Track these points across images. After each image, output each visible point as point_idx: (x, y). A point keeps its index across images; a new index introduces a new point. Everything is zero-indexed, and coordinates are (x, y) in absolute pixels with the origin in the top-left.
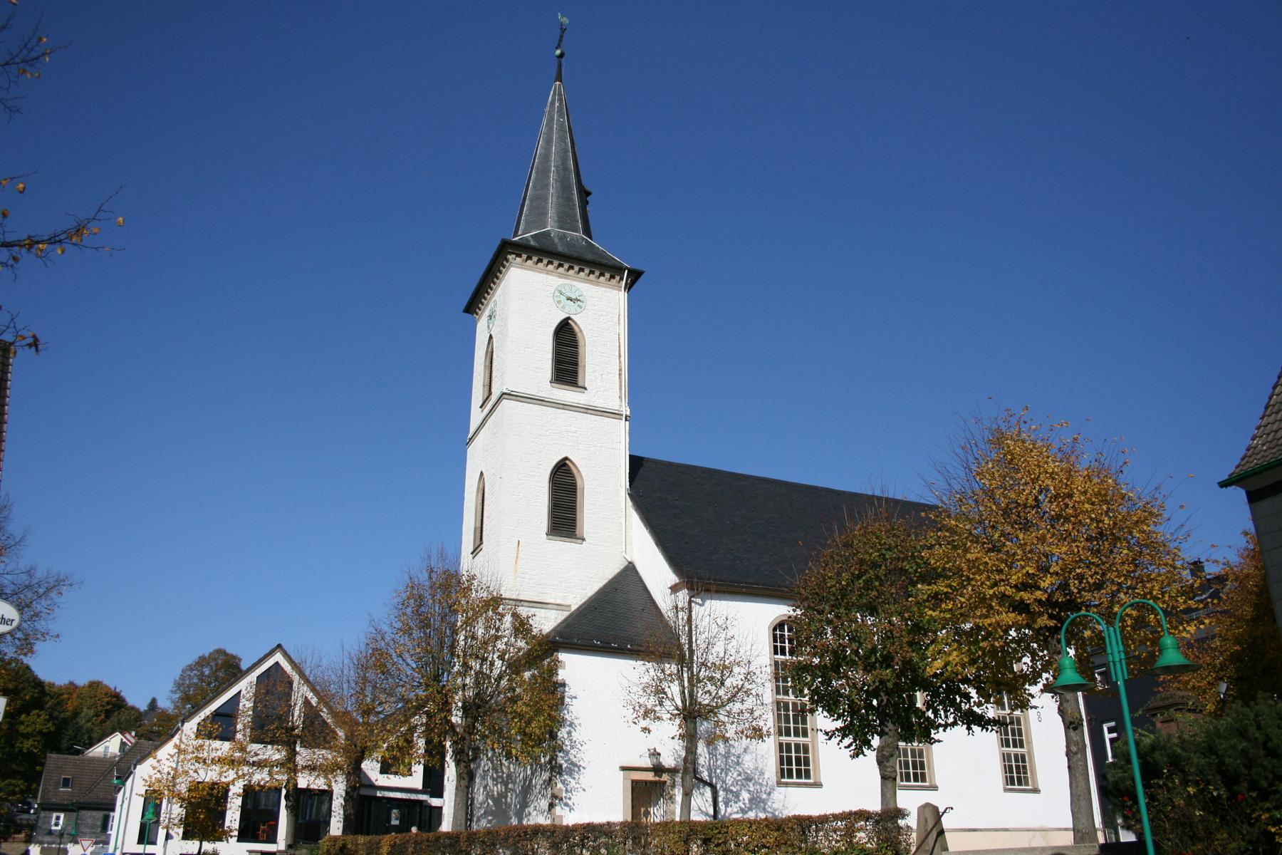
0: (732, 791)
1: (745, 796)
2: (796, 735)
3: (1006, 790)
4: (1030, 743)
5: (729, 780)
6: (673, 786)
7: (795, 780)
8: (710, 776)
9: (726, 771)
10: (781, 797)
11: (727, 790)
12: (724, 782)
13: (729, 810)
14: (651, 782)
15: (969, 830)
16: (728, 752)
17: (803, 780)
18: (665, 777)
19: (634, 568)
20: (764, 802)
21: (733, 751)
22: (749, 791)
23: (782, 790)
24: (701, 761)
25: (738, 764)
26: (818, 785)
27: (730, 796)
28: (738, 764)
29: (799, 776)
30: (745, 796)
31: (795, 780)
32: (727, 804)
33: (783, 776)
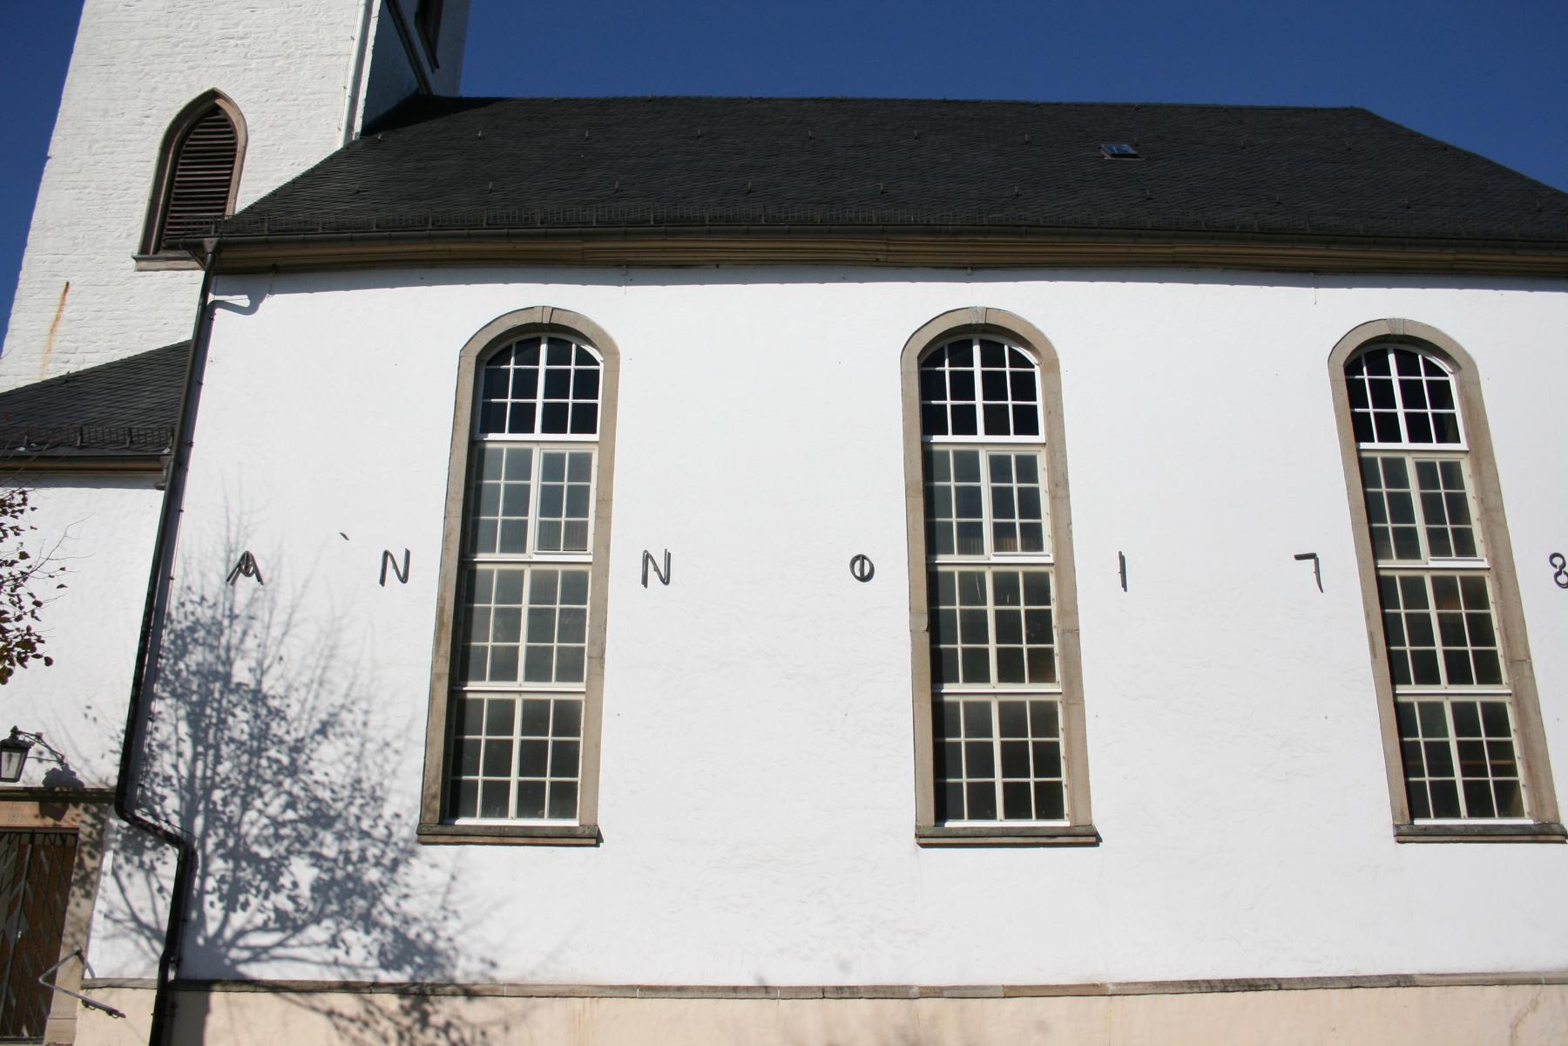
0: (255, 859)
1: (302, 872)
2: (1010, 671)
3: (1405, 834)
4: (1522, 662)
5: (253, 824)
6: (99, 846)
7: (1000, 822)
8: (187, 817)
9: (248, 794)
10: (439, 878)
11: (238, 854)
12: (232, 826)
13: (238, 919)
14: (33, 832)
15: (1228, 986)
16: (262, 735)
17: (546, 822)
18: (75, 817)
19: (144, 249)
20: (372, 894)
21: (277, 728)
22: (317, 859)
23: (444, 854)
24: (164, 764)
25: (293, 771)
26: (1087, 837)
27: (247, 874)
28: (293, 771)
29: (530, 801)
30: (302, 872)
31: (1000, 822)
32: (231, 902)
33: (1413, 814)
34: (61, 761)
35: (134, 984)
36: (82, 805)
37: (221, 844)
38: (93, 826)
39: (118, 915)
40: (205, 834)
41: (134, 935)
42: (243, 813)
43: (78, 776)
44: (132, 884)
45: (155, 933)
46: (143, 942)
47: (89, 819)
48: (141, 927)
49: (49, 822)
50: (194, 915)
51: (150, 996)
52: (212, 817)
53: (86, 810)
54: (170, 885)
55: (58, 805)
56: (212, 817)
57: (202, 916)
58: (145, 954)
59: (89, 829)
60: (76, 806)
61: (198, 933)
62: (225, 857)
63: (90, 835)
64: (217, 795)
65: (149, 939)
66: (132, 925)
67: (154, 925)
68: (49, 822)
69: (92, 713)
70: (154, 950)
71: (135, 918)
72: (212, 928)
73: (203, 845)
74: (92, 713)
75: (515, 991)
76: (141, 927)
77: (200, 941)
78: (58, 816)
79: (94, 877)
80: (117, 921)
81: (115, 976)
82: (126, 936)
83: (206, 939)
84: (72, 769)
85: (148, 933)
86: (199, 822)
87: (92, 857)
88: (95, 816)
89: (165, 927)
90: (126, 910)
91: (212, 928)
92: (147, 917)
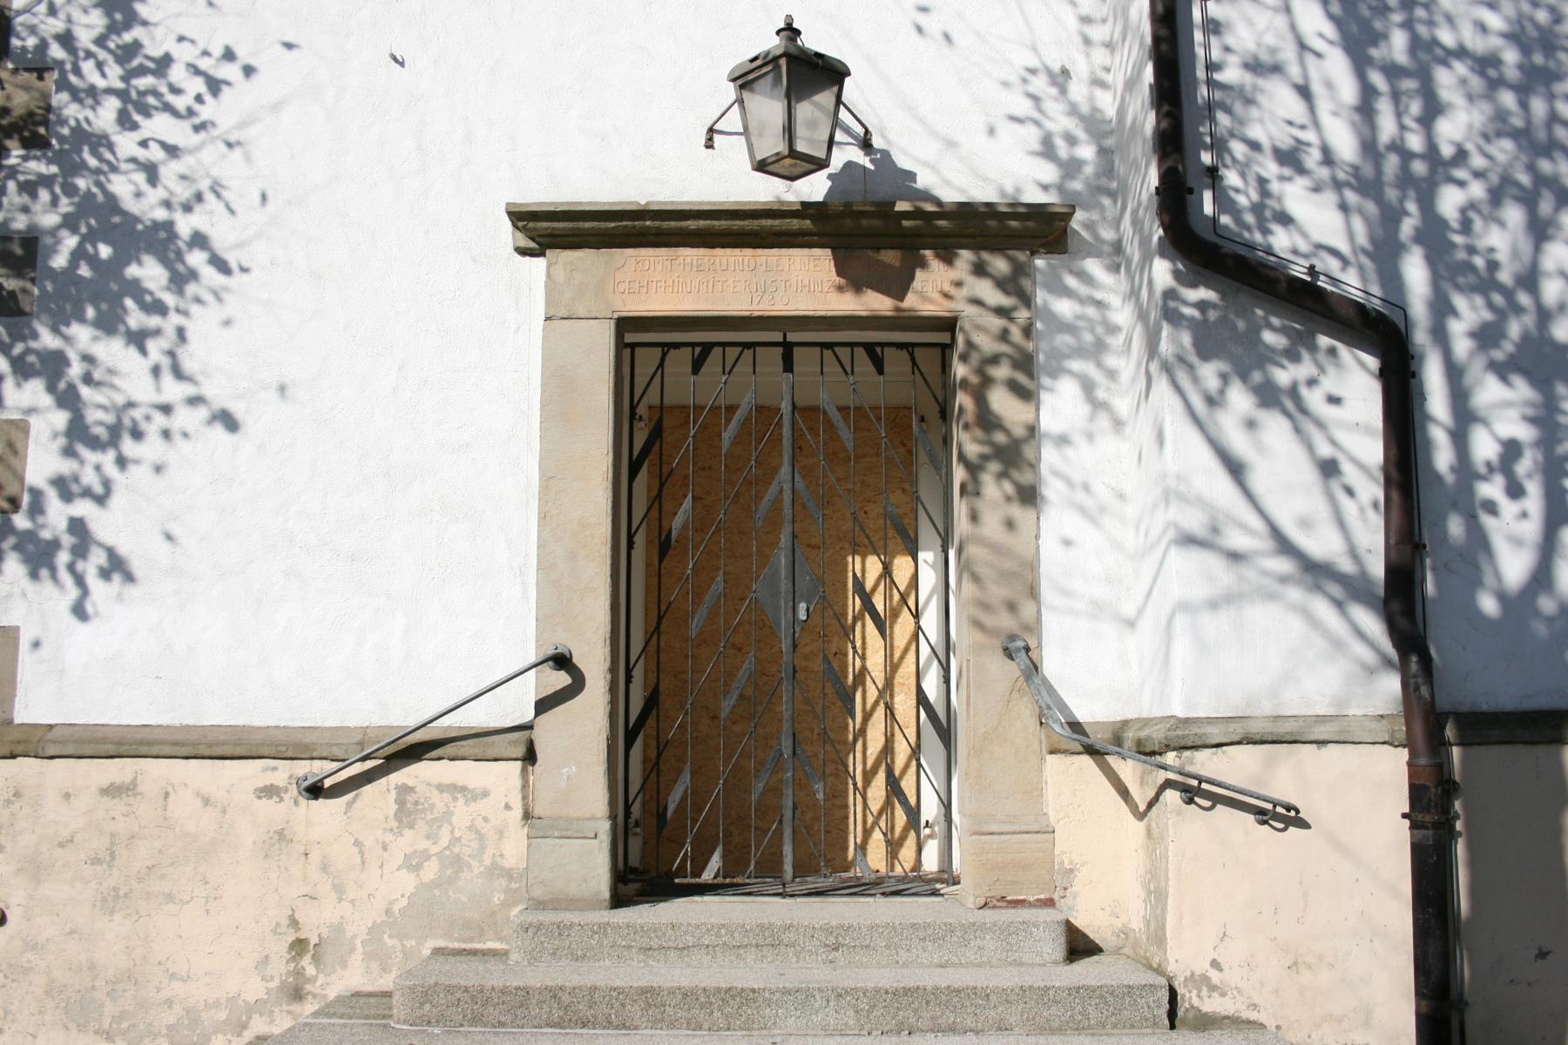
34: (866, 144)
35: (1320, 732)
36: (966, 256)
37: (1486, 336)
38: (1001, 312)
39: (1237, 540)
40: (1442, 309)
41: (1295, 594)
42: (1537, 249)
43: (923, 181)
44: (1261, 448)
45: (1352, 588)
46: (1323, 609)
47: (994, 297)
48: (1315, 572)
49: (877, 303)
50: (1455, 527)
51: (1386, 774)
52: (1451, 270)
53: (980, 270)
54: (1372, 450)
55: (890, 257)
56: (1451, 270)
57: (1479, 542)
58: (1338, 644)
59: (997, 323)
60: (948, 259)
61: (1476, 583)
62: (1502, 371)
63: (1004, 336)
64: (1450, 201)
65: (1339, 605)
66: (1283, 565)
67: (1346, 566)
68: (877, 303)
69: (931, 23)
70: (1360, 634)
71: (1284, 546)
72: (1514, 566)
73: (1440, 336)
74: (931, 23)
75: (1237, 731)
76: (1315, 572)
77: (1488, 604)
78: (898, 286)
79: (1028, 452)
80: (1235, 557)
81: (1267, 709)
82: (1270, 596)
83: (1502, 597)
84: (903, 162)
85: (1336, 590)
86: (1415, 273)
87: (1025, 394)
88: (1002, 284)
89: (1377, 569)
90: (1256, 522)
91: (1514, 566)
92: (1323, 544)
